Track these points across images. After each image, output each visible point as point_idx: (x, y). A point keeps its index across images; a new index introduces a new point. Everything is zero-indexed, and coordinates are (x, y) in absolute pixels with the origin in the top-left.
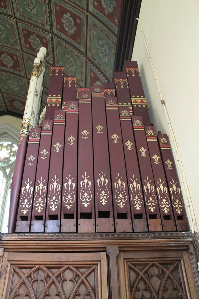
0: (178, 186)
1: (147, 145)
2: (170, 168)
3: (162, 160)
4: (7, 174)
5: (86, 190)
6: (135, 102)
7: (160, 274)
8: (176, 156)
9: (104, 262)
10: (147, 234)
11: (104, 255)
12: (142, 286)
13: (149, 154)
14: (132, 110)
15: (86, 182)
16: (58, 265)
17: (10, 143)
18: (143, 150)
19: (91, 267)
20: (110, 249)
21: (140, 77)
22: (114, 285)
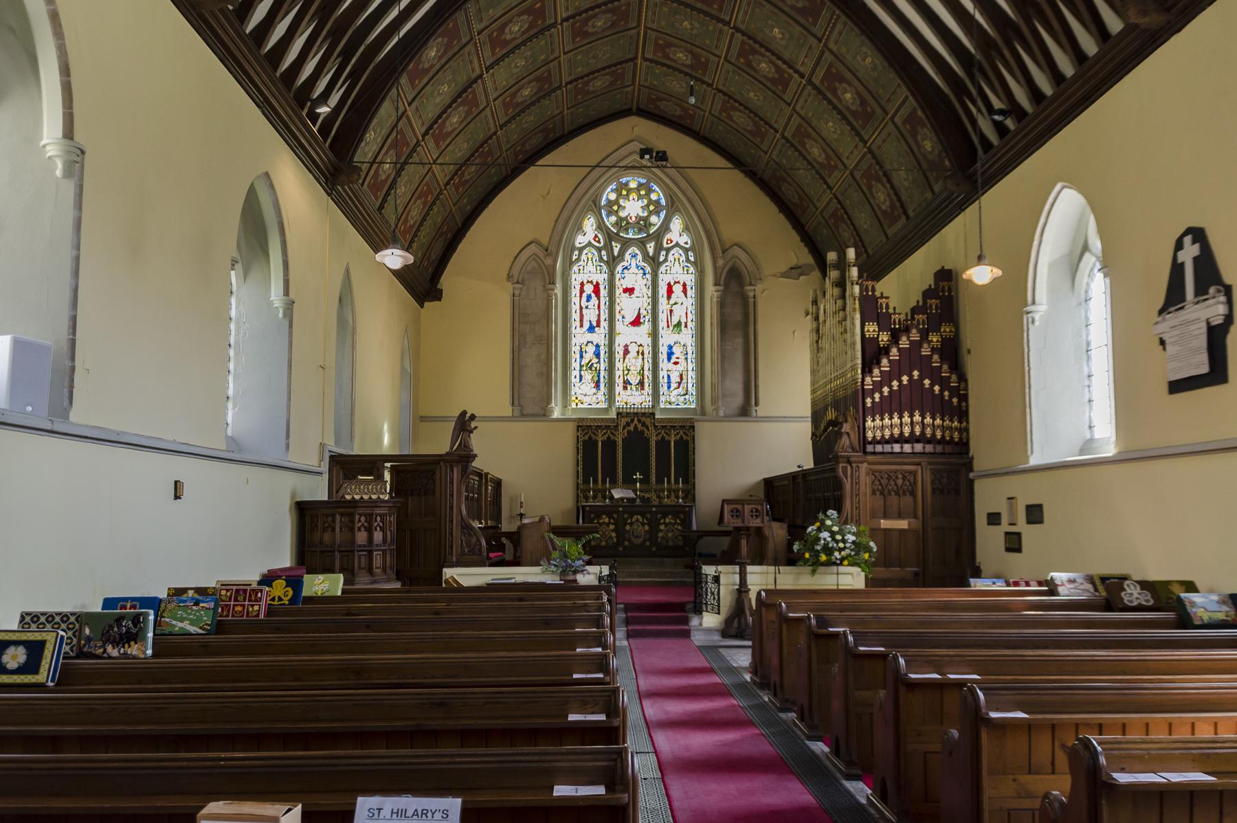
0: (968, 422)
1: (951, 389)
2: (964, 408)
3: (959, 402)
4: (651, 254)
5: (906, 425)
6: (945, 331)
7: (547, 282)
8: (971, 402)
9: (920, 471)
10: (734, 70)
11: (919, 467)
12: (877, 483)
13: (951, 397)
14: (984, 736)
15: (906, 419)
16: (896, 472)
17: (643, 181)
18: (946, 393)
19: (914, 473)
20: (923, 464)
21: (952, 296)
22: (925, 481)
